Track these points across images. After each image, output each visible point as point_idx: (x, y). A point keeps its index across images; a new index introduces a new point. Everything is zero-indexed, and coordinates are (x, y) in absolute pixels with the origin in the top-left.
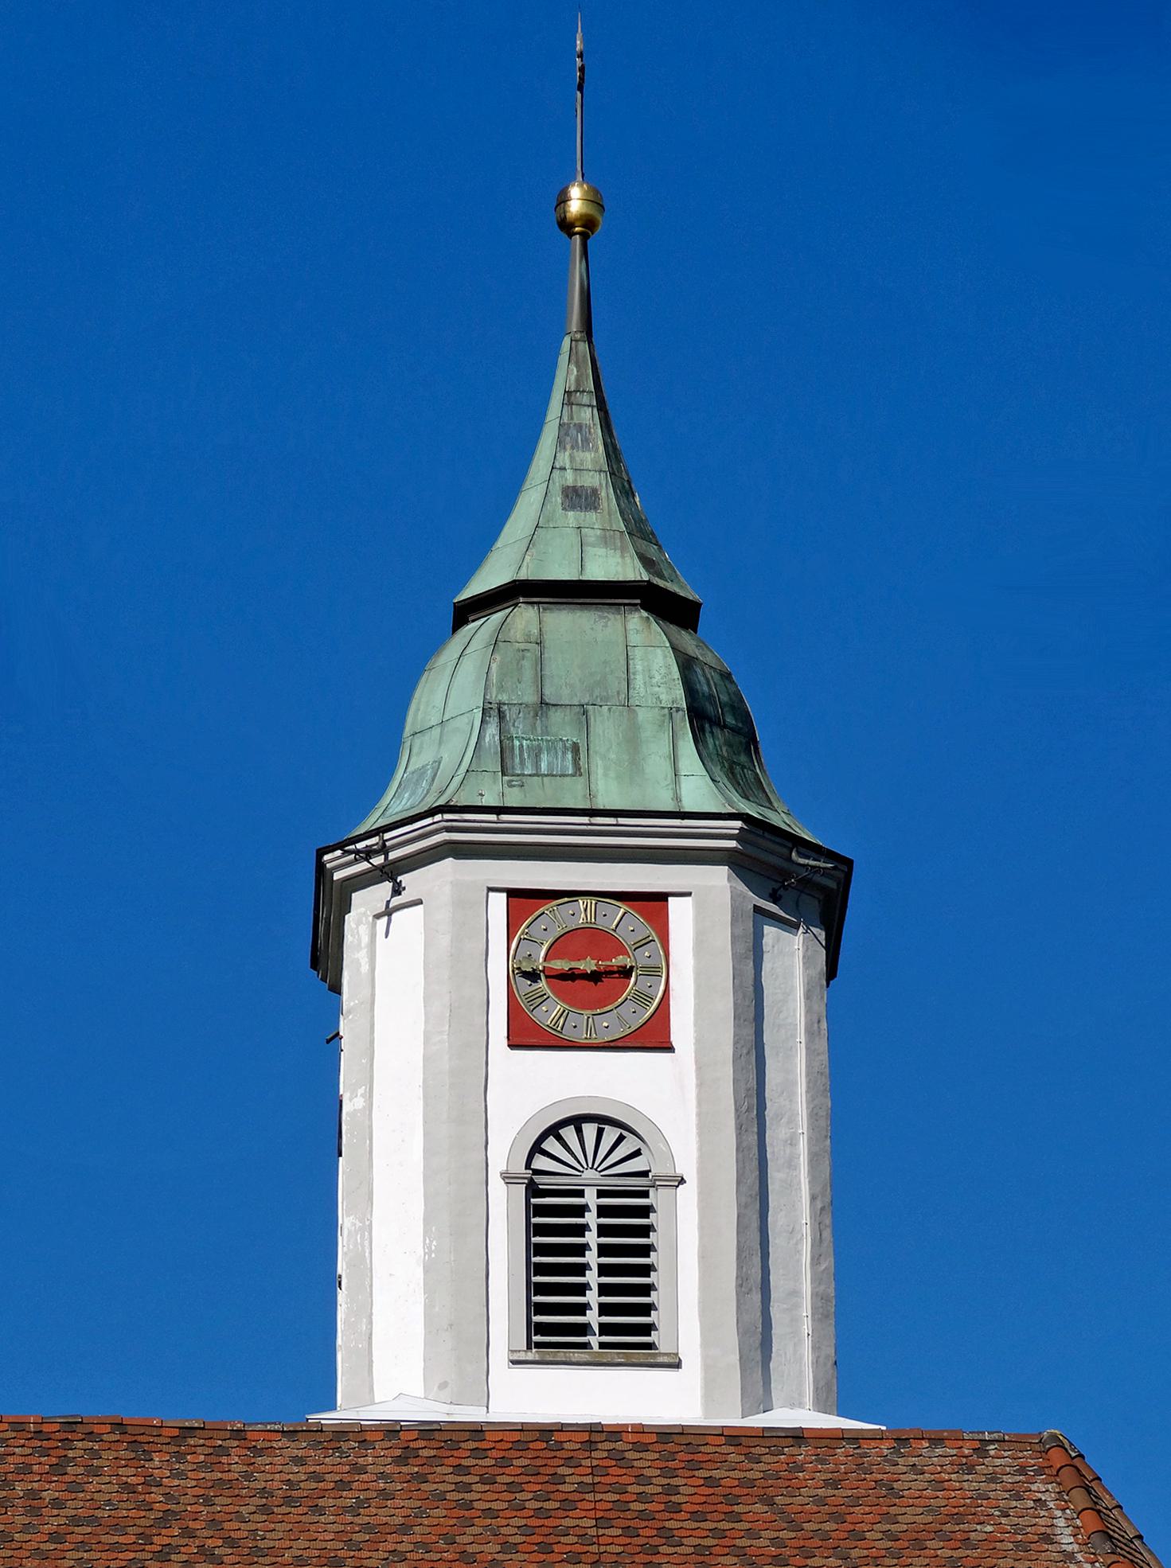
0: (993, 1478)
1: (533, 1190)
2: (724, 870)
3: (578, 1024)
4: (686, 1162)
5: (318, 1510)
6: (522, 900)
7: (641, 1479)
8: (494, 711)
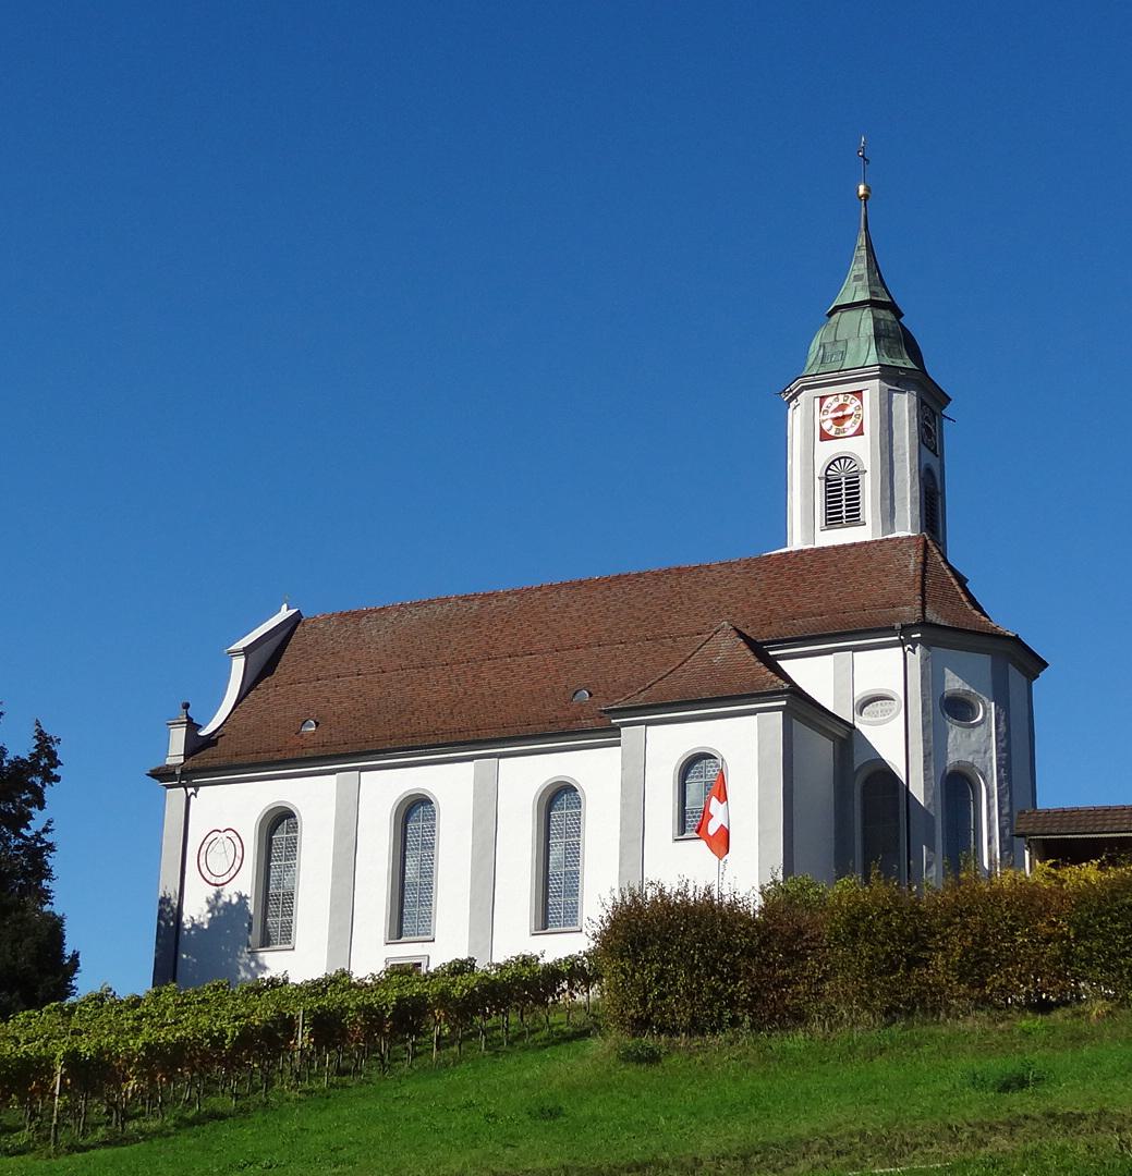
1: (827, 480)
2: (877, 382)
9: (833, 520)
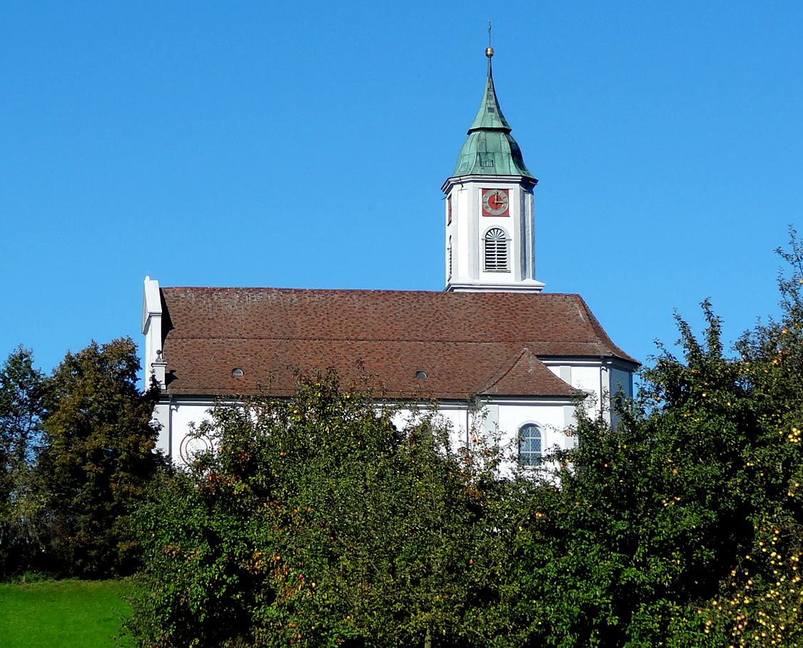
0: (568, 303)
1: (486, 241)
2: (518, 185)
3: (494, 212)
4: (512, 236)
5: (461, 309)
6: (485, 190)
7: (512, 303)
8: (478, 154)
9: (489, 267)
